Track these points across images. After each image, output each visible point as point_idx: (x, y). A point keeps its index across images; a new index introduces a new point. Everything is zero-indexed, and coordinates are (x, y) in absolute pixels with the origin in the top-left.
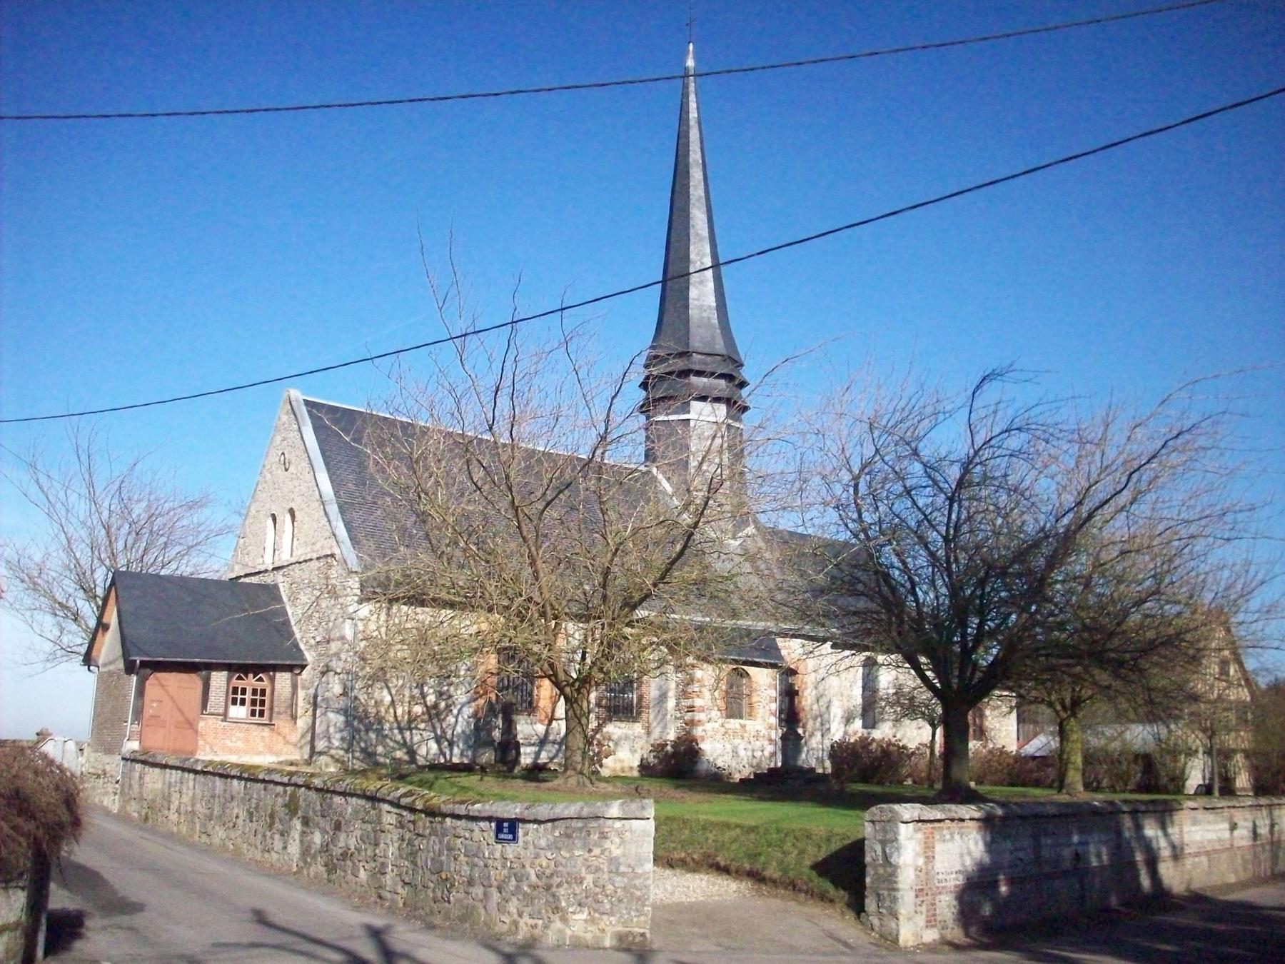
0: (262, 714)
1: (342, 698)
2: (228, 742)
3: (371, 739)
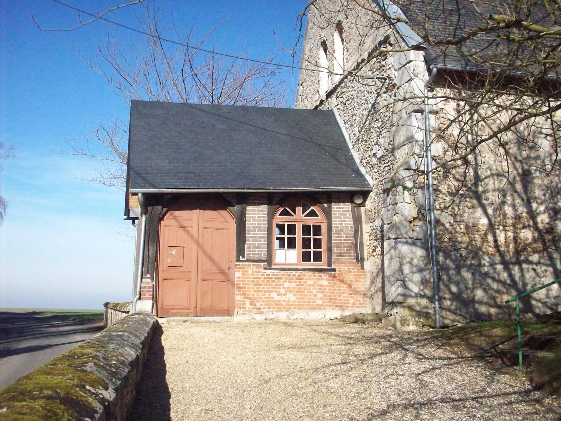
0: (317, 257)
1: (418, 223)
2: (274, 295)
3: (464, 280)
